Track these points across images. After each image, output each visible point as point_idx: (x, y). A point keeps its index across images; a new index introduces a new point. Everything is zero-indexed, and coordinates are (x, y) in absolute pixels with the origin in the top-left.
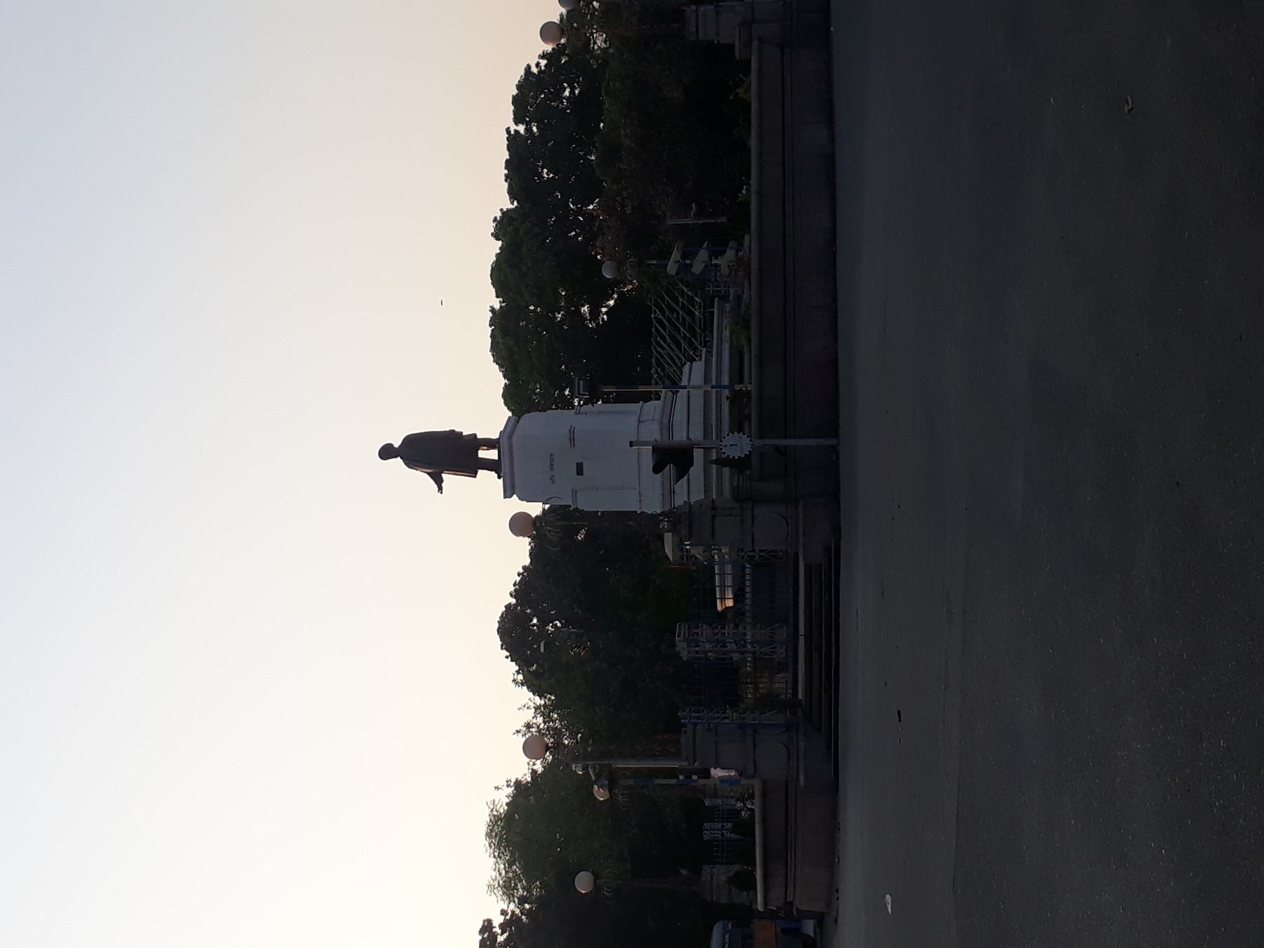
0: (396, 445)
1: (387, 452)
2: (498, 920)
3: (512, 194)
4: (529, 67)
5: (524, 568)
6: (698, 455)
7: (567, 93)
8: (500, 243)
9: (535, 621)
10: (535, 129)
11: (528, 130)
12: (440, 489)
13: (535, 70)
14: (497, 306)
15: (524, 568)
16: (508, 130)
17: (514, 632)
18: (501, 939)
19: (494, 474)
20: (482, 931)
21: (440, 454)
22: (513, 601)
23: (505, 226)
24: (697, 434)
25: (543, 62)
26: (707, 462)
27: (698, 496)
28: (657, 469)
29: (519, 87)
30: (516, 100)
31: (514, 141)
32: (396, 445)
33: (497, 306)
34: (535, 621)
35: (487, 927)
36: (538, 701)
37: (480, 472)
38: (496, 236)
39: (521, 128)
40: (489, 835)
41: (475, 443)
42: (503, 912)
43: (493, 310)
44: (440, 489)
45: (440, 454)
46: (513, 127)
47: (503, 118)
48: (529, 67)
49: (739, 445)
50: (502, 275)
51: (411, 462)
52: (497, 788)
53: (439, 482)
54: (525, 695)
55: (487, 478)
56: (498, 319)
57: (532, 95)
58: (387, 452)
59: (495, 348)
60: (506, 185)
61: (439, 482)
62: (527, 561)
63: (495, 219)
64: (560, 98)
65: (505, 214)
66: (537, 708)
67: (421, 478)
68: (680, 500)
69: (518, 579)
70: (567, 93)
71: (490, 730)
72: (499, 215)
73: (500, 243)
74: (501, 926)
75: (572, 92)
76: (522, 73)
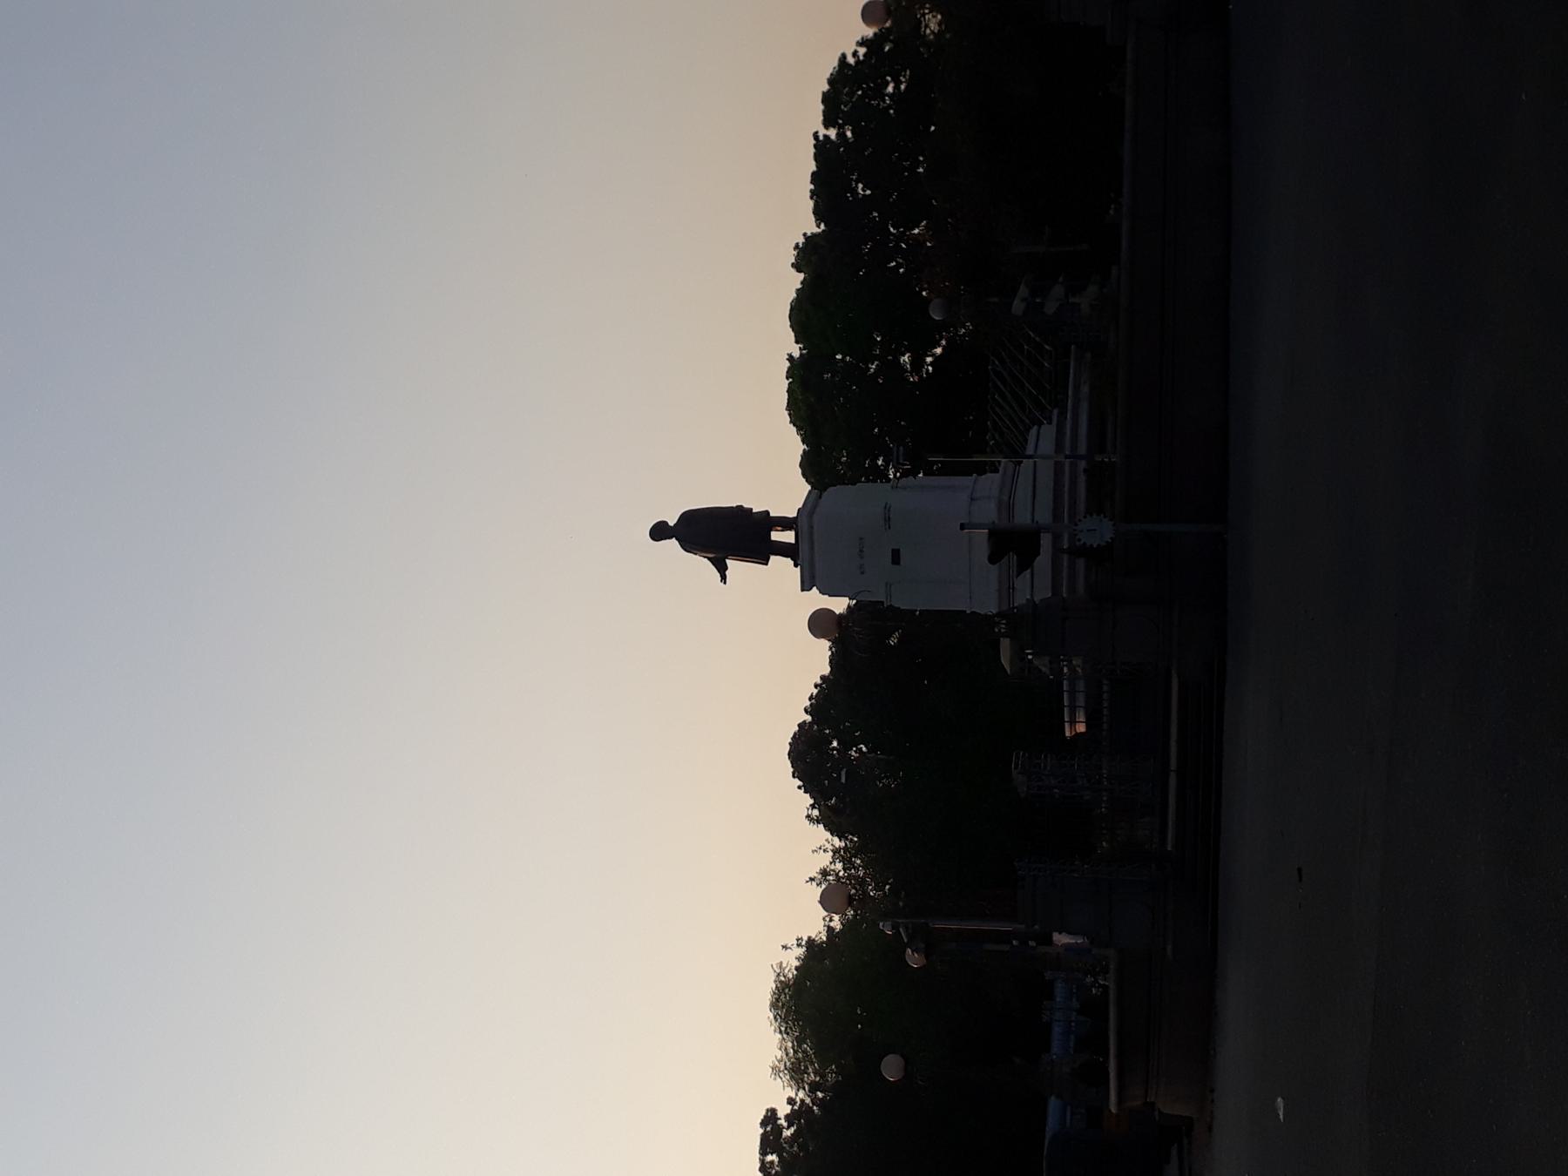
0: (671, 524)
1: (660, 532)
2: (784, 1110)
3: (819, 214)
4: (844, 56)
5: (822, 678)
6: (1046, 541)
7: (890, 89)
8: (802, 276)
9: (835, 744)
10: (849, 134)
11: (841, 135)
12: (724, 578)
13: (851, 60)
14: (796, 354)
15: (822, 678)
16: (816, 135)
17: (810, 756)
18: (787, 1133)
19: (789, 562)
20: (764, 1124)
21: (722, 535)
22: (809, 718)
23: (809, 255)
24: (1044, 516)
25: (862, 51)
26: (1057, 550)
27: (1044, 592)
28: (994, 559)
29: (831, 81)
30: (826, 99)
31: (823, 148)
32: (671, 524)
33: (796, 354)
34: (835, 744)
35: (770, 1117)
36: (837, 842)
37: (773, 558)
38: (797, 267)
39: (832, 133)
40: (774, 1005)
41: (768, 522)
42: (791, 1101)
43: (791, 358)
44: (724, 578)
45: (722, 535)
46: (822, 132)
47: (812, 119)
48: (844, 56)
49: (1099, 531)
50: (803, 316)
51: (689, 545)
52: (785, 947)
53: (722, 570)
54: (821, 834)
55: (781, 566)
56: (799, 372)
57: (847, 91)
58: (660, 532)
59: (792, 406)
60: (811, 203)
61: (722, 570)
62: (827, 670)
63: (797, 247)
64: (882, 96)
65: (809, 239)
66: (836, 851)
67: (701, 565)
68: (1020, 599)
69: (815, 691)
70: (890, 89)
71: (775, 878)
72: (801, 240)
73: (802, 276)
74: (787, 1117)
75: (897, 87)
76: (836, 63)
